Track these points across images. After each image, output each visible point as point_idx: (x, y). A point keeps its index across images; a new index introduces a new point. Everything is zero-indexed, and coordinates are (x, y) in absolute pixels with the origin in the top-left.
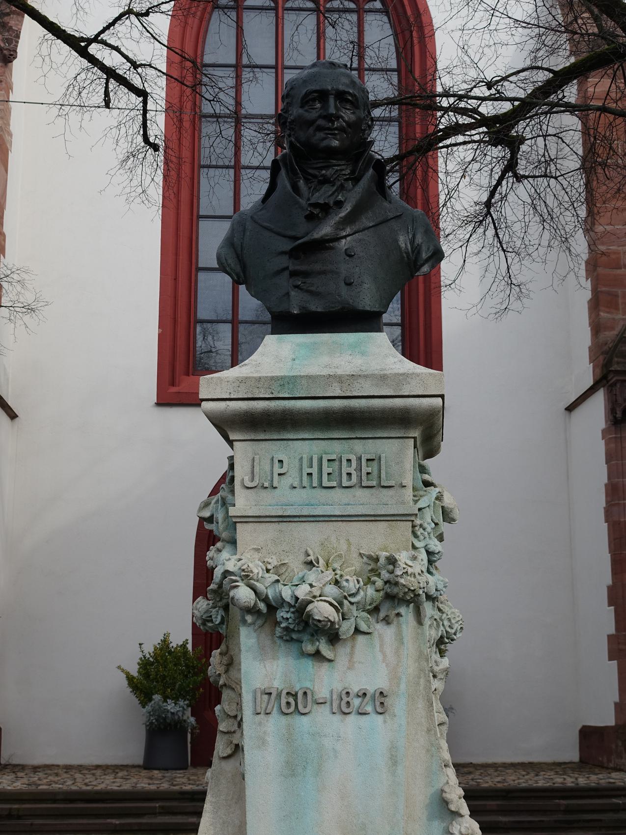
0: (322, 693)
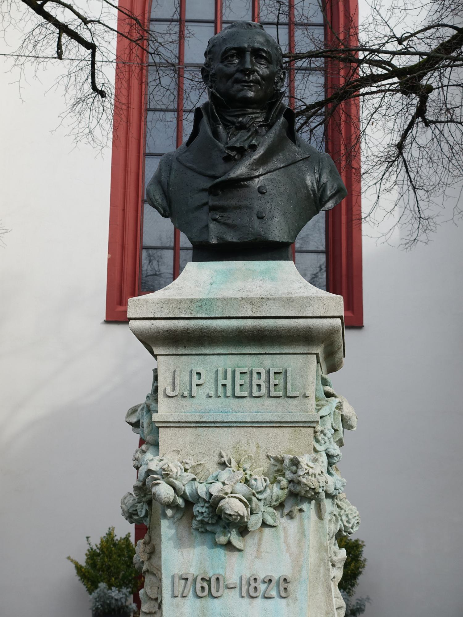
0: (233, 579)
